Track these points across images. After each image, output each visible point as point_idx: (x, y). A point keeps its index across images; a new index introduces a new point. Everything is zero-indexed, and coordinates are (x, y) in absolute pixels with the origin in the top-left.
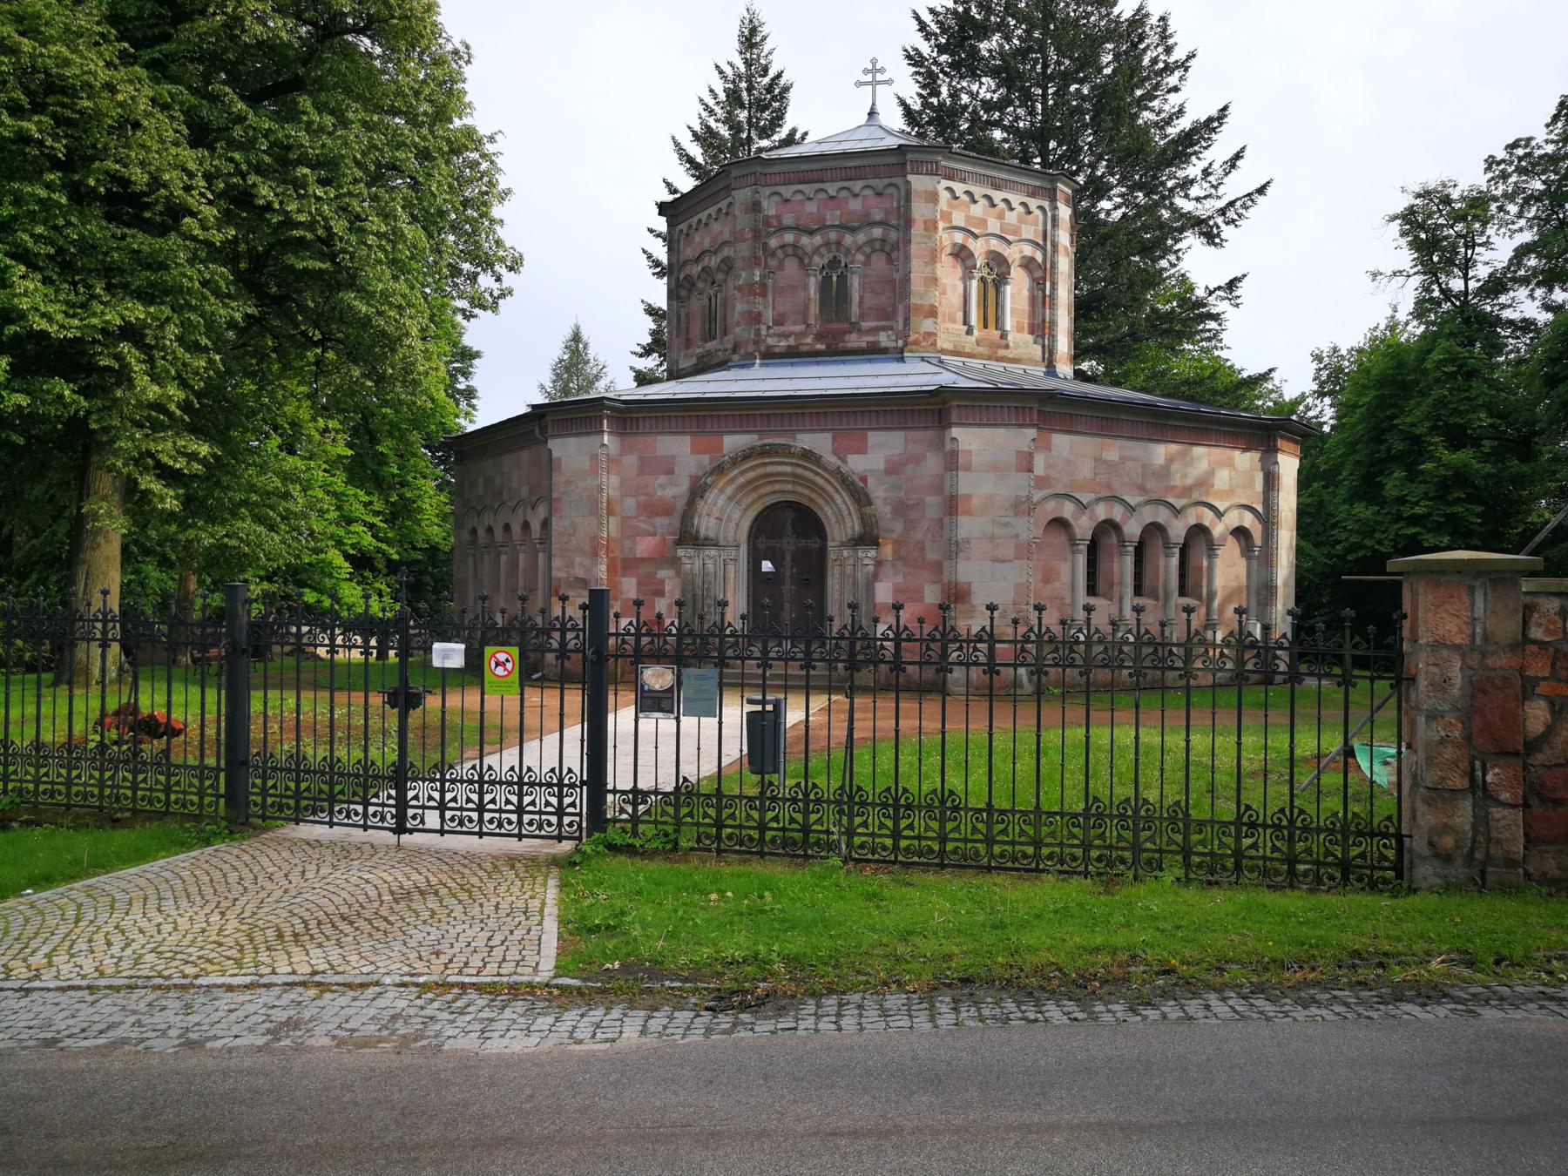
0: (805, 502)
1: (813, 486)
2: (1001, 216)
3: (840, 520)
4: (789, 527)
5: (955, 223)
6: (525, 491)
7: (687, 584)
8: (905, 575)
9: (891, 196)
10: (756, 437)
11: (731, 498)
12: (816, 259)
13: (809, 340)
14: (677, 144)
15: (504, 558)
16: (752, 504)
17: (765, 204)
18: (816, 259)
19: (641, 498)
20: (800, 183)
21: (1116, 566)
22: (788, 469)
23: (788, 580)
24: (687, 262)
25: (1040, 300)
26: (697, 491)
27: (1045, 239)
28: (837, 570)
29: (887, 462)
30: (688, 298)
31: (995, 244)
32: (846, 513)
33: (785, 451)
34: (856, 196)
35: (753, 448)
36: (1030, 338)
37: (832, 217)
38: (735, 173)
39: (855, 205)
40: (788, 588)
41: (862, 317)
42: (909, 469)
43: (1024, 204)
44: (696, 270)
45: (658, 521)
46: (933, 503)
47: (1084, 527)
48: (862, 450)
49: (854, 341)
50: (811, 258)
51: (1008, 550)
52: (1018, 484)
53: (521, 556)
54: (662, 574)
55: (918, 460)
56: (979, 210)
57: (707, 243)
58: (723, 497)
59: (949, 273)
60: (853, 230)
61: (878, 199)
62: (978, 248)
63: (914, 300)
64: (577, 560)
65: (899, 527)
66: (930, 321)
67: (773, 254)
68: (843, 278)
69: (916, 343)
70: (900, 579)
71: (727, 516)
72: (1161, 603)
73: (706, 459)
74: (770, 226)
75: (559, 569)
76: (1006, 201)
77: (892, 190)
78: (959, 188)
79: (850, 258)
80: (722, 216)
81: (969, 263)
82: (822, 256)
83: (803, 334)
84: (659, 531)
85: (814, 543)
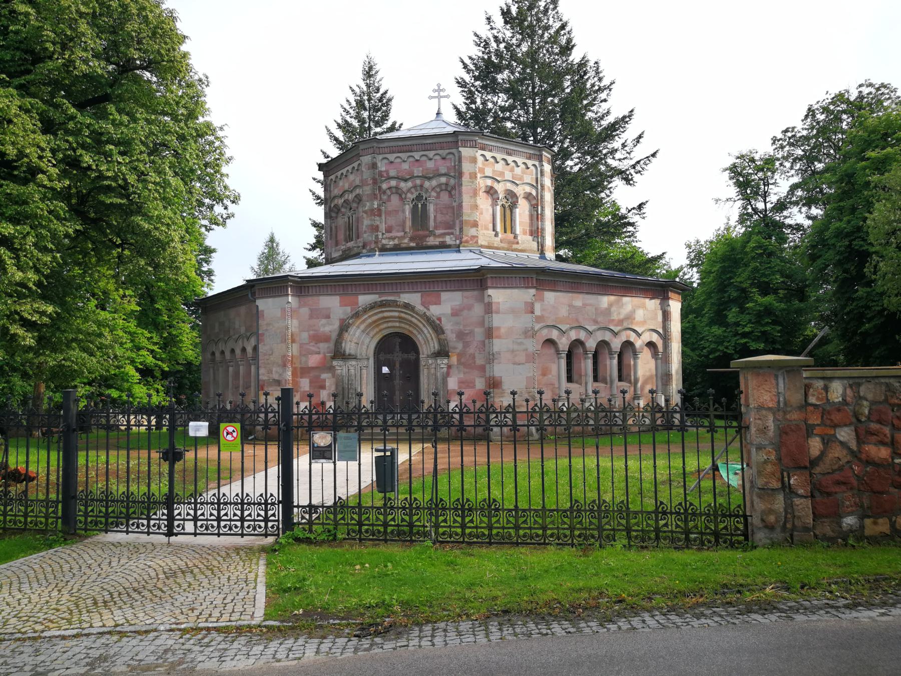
0: (407, 333)
1: (411, 323)
2: (512, 170)
3: (427, 343)
5: (486, 174)
6: (243, 330)
7: (339, 382)
11: (363, 331)
12: (409, 195)
15: (231, 369)
16: (377, 333)
17: (379, 164)
18: (409, 195)
19: (311, 332)
22: (396, 314)
23: (398, 377)
24: (335, 197)
27: (537, 183)
29: (452, 309)
30: (336, 217)
31: (509, 186)
32: (430, 338)
33: (394, 304)
34: (431, 159)
36: (531, 238)
37: (418, 171)
38: (362, 147)
39: (430, 165)
40: (398, 382)
41: (436, 227)
42: (465, 313)
44: (340, 201)
46: (479, 332)
47: (564, 344)
48: (438, 303)
49: (431, 241)
50: (406, 194)
51: (522, 358)
52: (526, 321)
53: (241, 367)
54: (324, 376)
55: (470, 308)
56: (500, 166)
57: (346, 187)
58: (359, 331)
59: (484, 202)
60: (429, 179)
62: (500, 188)
63: (465, 218)
64: (274, 369)
65: (460, 346)
67: (384, 192)
68: (424, 206)
69: (467, 242)
70: (462, 376)
73: (348, 309)
74: (382, 176)
76: (514, 161)
77: (451, 156)
78: (488, 155)
81: (495, 196)
82: (412, 193)
84: (322, 351)
85: (412, 356)
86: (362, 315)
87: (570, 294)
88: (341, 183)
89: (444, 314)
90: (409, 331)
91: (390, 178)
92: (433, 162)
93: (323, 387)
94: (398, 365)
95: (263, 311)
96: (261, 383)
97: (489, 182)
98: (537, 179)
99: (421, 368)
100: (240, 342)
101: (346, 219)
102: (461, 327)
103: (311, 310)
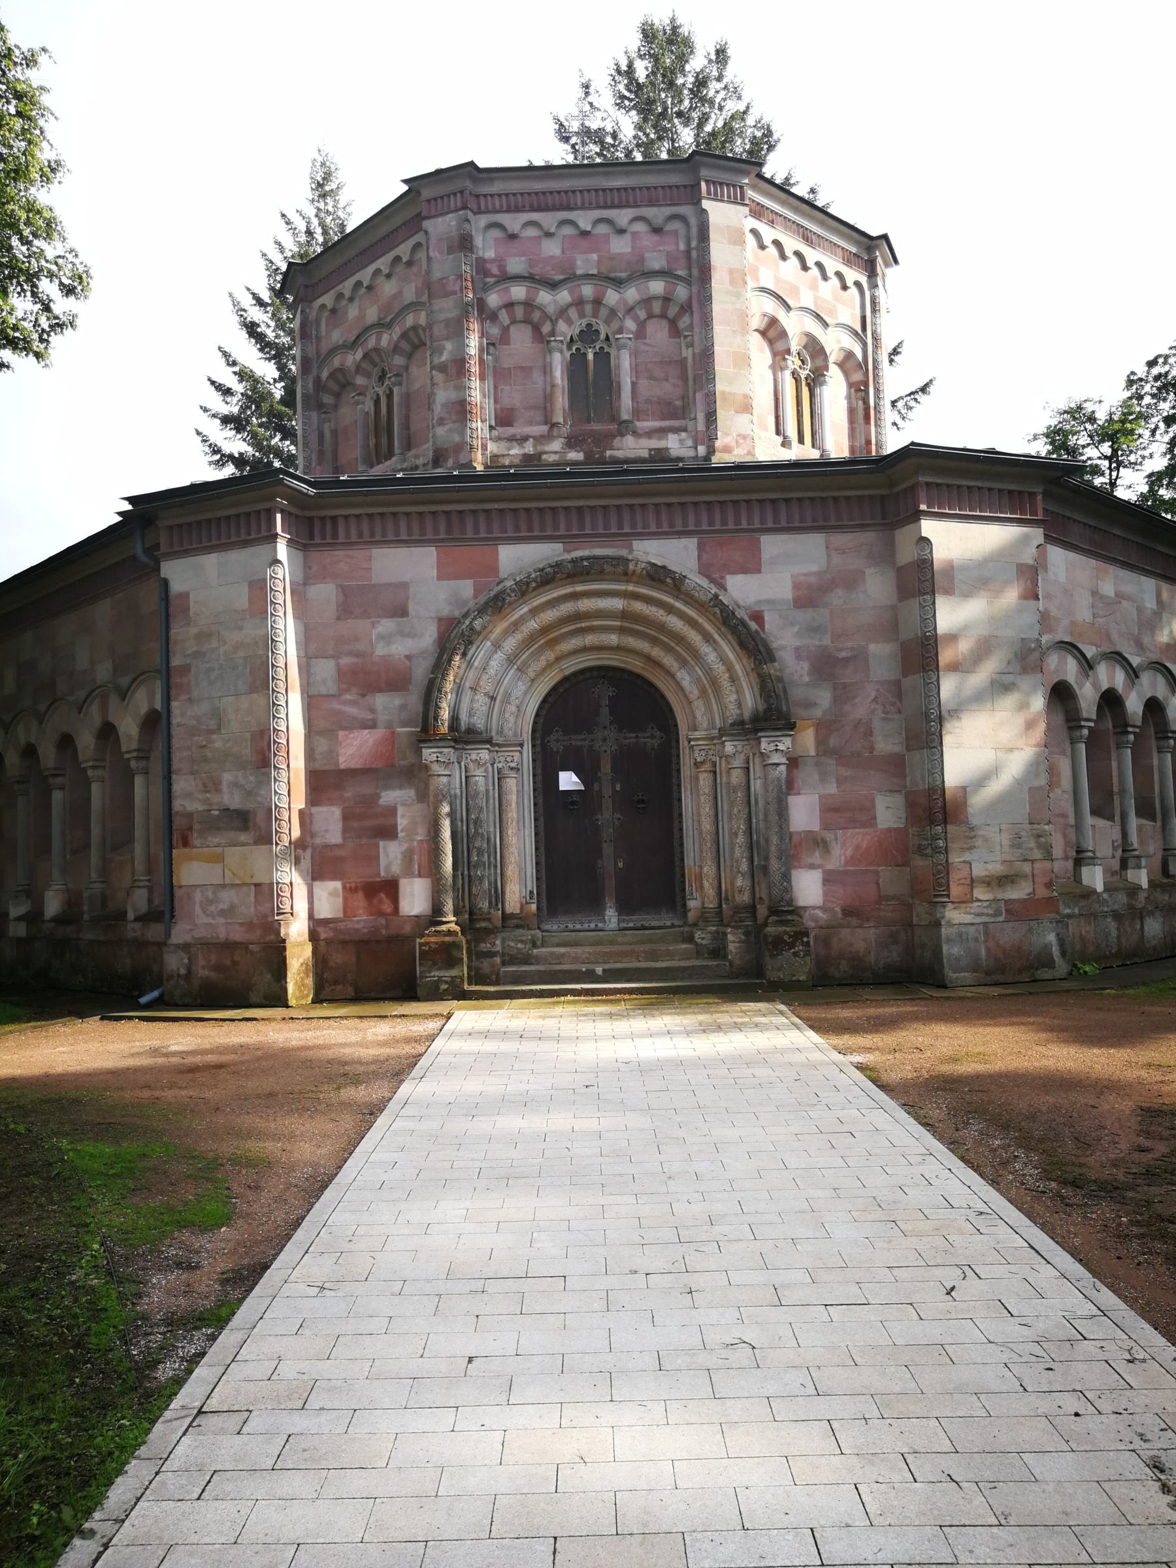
0: (635, 665)
1: (658, 633)
3: (706, 690)
4: (605, 711)
6: (103, 672)
8: (840, 781)
9: (675, 233)
10: (559, 547)
11: (511, 660)
12: (562, 326)
13: (557, 445)
14: (235, 303)
15: (57, 796)
16: (549, 666)
17: (478, 241)
18: (562, 326)
19: (346, 661)
20: (533, 209)
21: (1114, 765)
22: (618, 604)
23: (607, 803)
24: (333, 351)
25: (861, 413)
26: (454, 638)
28: (705, 780)
29: (796, 586)
30: (336, 407)
32: (724, 679)
33: (619, 569)
34: (621, 232)
35: (558, 565)
37: (585, 263)
38: (427, 193)
39: (620, 246)
40: (608, 816)
41: (637, 413)
42: (837, 597)
43: (839, 275)
44: (352, 358)
45: (381, 701)
46: (881, 655)
48: (752, 566)
50: (554, 323)
53: (95, 787)
54: (389, 797)
55: (851, 581)
58: (499, 657)
59: (760, 354)
60: (618, 283)
61: (655, 238)
62: (795, 326)
63: (720, 387)
64: (227, 777)
65: (824, 698)
66: (744, 418)
70: (832, 789)
71: (501, 687)
72: (1159, 823)
73: (466, 588)
74: (486, 273)
75: (188, 795)
77: (676, 225)
79: (615, 325)
80: (399, 269)
81: (780, 346)
82: (570, 322)
83: (548, 438)
84: (382, 718)
85: (651, 739)
86: (513, 605)
87: (1093, 562)
88: (353, 312)
89: (768, 601)
90: (648, 658)
91: (507, 278)
92: (627, 238)
93: (389, 833)
94: (606, 767)
95: (185, 595)
96: (178, 822)
97: (770, 306)
98: (864, 318)
99: (686, 771)
100: (94, 710)
101: (369, 406)
102: (827, 641)
103: (344, 590)
